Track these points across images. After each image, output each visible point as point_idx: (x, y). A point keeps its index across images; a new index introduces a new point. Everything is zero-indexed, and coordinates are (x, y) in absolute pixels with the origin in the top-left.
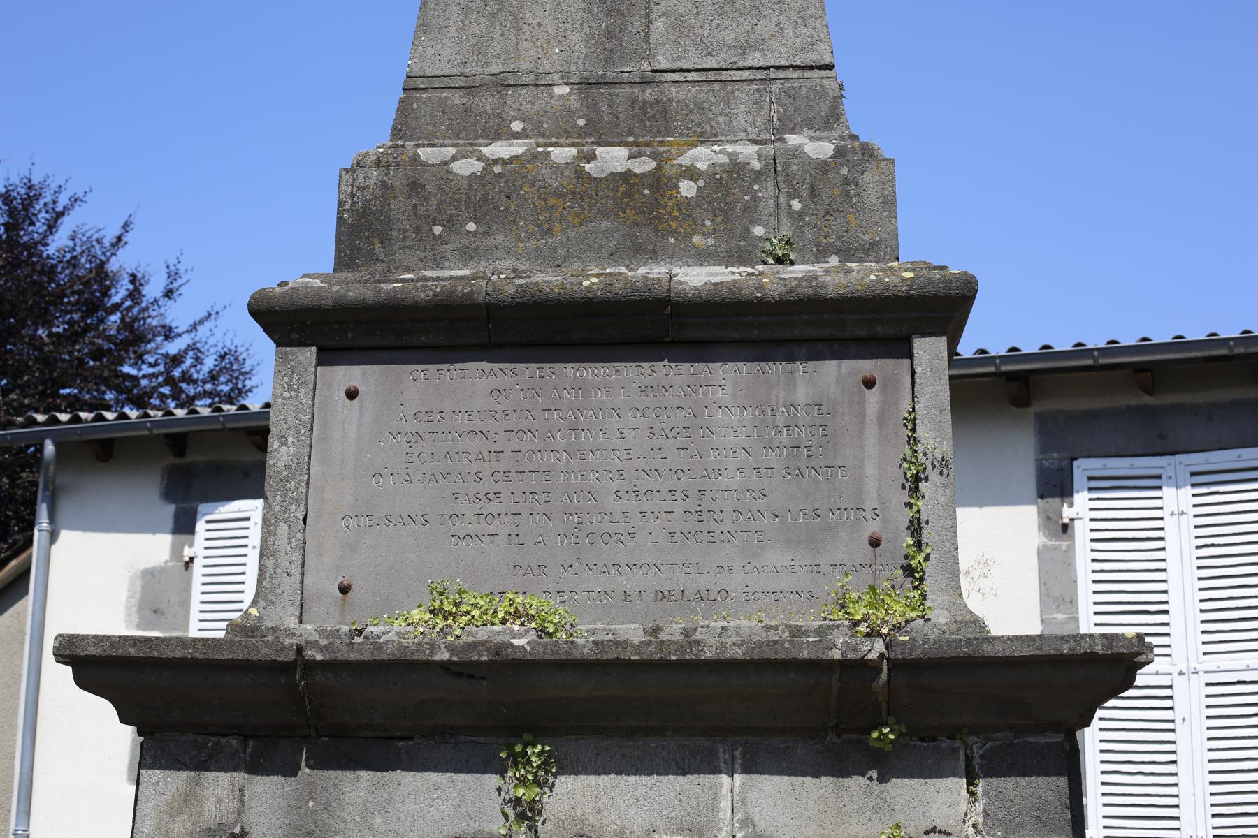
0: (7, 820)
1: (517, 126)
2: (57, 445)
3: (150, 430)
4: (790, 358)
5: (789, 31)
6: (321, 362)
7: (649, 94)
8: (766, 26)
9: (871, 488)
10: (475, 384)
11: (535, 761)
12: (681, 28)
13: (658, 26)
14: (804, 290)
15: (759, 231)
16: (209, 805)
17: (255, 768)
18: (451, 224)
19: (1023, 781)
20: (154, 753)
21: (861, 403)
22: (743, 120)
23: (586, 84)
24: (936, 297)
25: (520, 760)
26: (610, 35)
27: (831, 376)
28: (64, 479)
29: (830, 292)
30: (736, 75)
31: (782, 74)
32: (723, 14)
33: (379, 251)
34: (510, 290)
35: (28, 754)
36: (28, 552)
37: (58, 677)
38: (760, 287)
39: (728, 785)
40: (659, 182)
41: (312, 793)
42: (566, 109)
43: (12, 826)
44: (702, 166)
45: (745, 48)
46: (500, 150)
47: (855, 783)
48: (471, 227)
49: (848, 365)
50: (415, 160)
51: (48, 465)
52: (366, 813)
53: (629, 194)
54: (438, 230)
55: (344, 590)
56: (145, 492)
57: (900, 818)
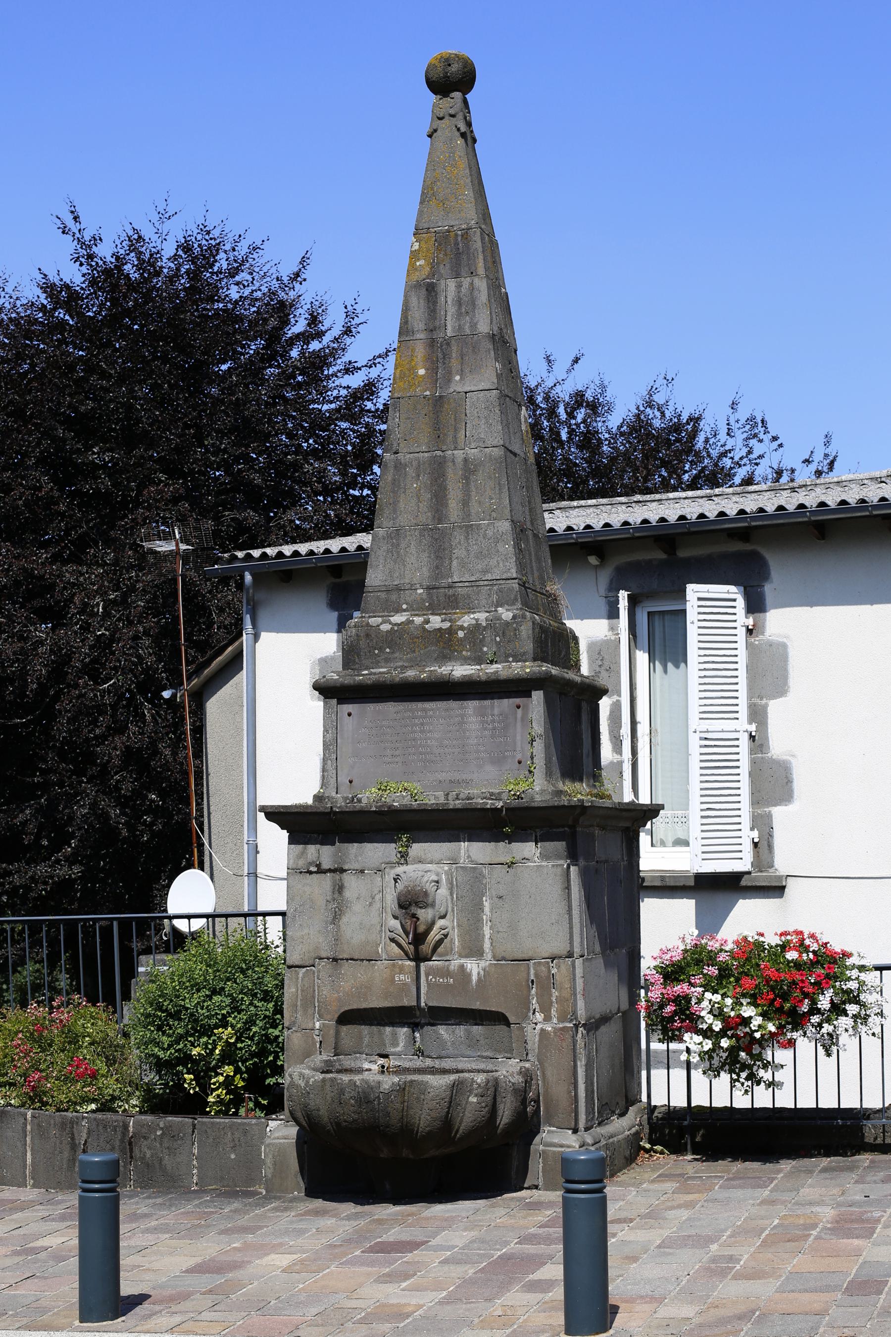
0: (242, 832)
1: (404, 606)
2: (252, 574)
3: (315, 563)
4: (492, 699)
5: (501, 565)
6: (338, 703)
7: (451, 592)
8: (493, 562)
9: (519, 744)
10: (391, 708)
11: (405, 840)
12: (463, 565)
13: (455, 563)
14: (493, 677)
15: (485, 649)
16: (309, 856)
17: (322, 844)
18: (381, 649)
19: (552, 843)
20: (293, 840)
21: (516, 713)
22: (484, 602)
23: (429, 588)
24: (537, 679)
25: (400, 839)
26: (437, 567)
27: (506, 704)
28: (260, 596)
29: (502, 678)
30: (482, 583)
31: (498, 582)
32: (477, 558)
33: (357, 660)
34: (397, 679)
35: (252, 789)
36: (240, 640)
37: (261, 816)
38: (479, 677)
39: (464, 845)
40: (451, 631)
41: (340, 851)
42: (421, 599)
43: (246, 838)
44: (466, 625)
45: (485, 572)
46: (398, 618)
47: (501, 844)
48: (388, 650)
49: (512, 700)
50: (368, 624)
51: (248, 589)
52: (356, 856)
53: (440, 636)
54: (376, 652)
55: (351, 782)
56: (317, 603)
57: (514, 855)
